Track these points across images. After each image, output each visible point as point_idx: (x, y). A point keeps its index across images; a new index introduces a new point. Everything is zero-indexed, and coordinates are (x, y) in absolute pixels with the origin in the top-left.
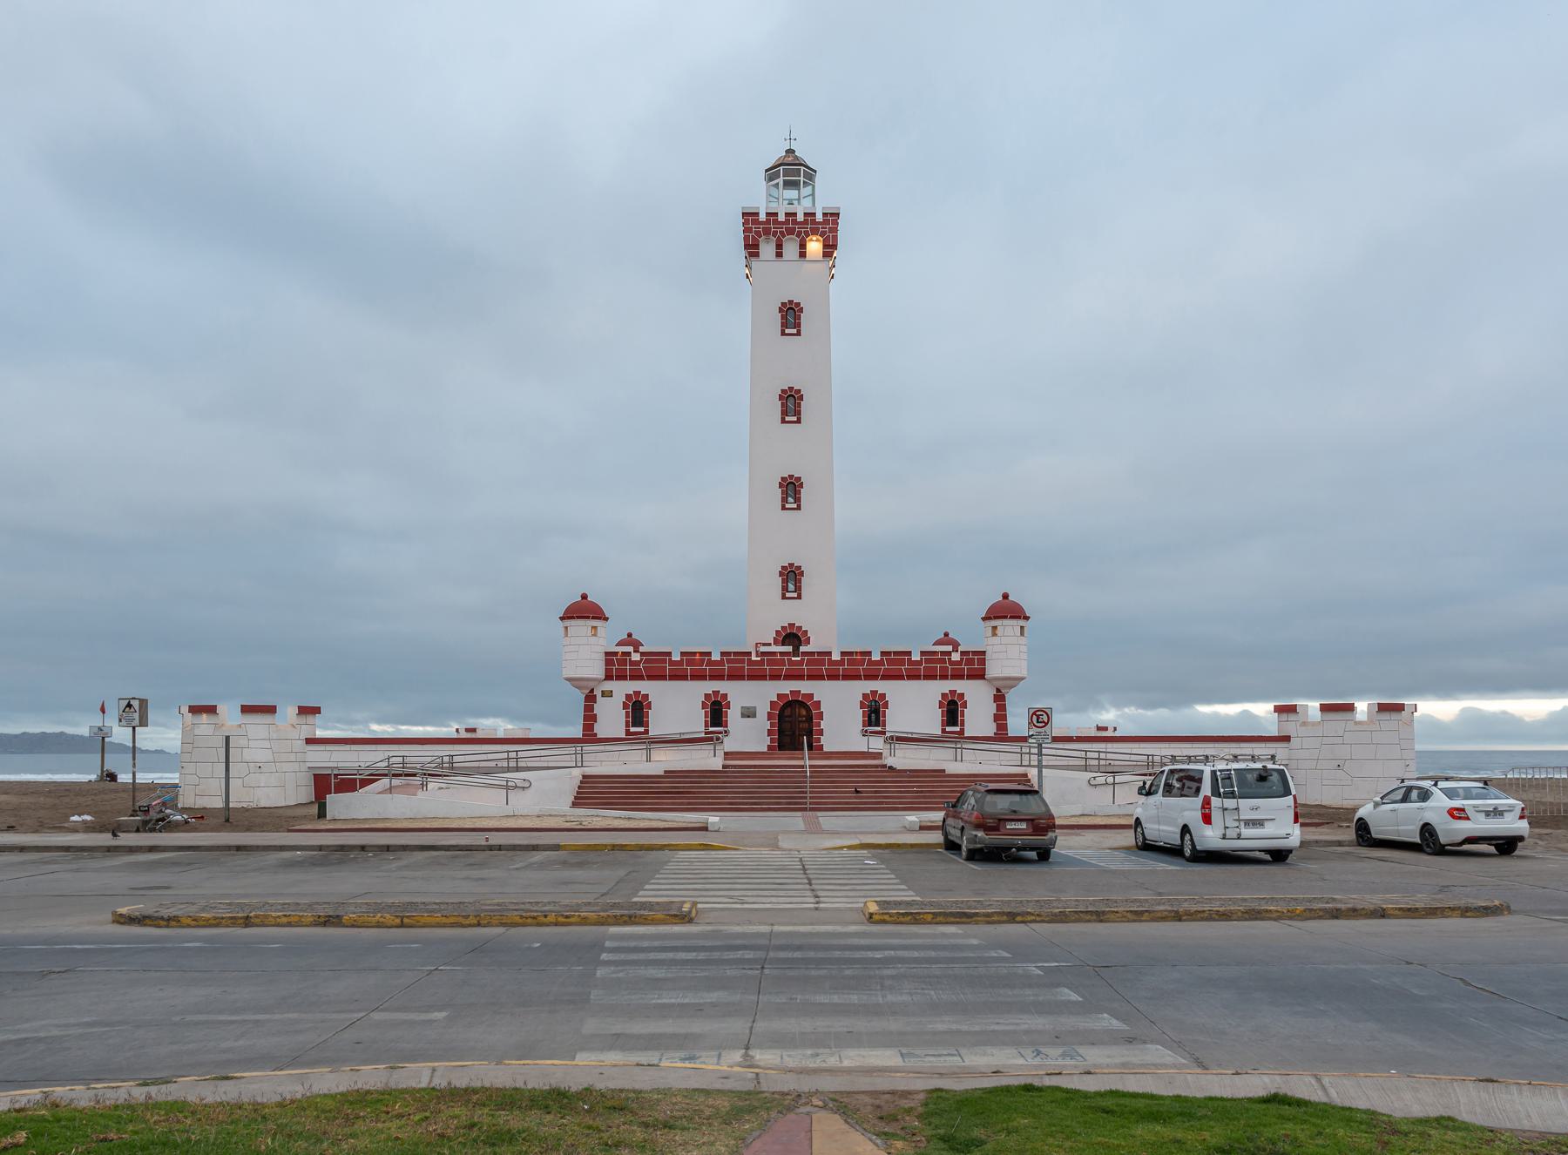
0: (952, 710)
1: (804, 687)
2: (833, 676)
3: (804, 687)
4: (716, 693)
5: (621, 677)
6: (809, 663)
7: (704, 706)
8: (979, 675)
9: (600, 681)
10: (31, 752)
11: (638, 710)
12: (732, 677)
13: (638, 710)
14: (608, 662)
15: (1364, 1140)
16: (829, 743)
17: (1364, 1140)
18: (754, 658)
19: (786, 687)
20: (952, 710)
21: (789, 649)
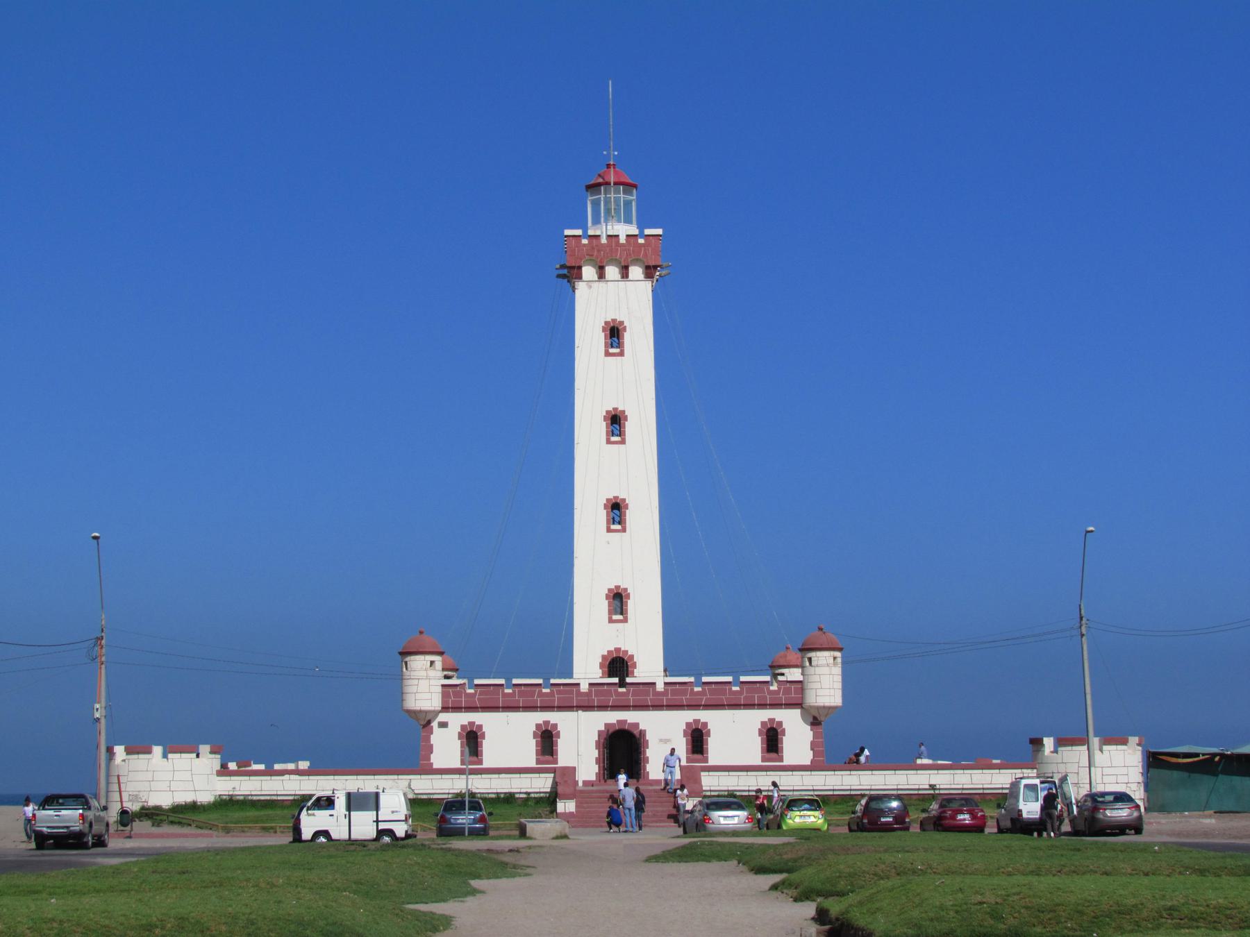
0: (772, 739)
1: (631, 717)
2: (658, 707)
3: (631, 717)
4: (471, 724)
5: (457, 709)
6: (521, 694)
7: (535, 735)
8: (798, 704)
9: (436, 713)
10: (572, 565)
11: (472, 739)
12: (561, 708)
13: (472, 739)
14: (445, 695)
15: (277, 767)
16: (651, 777)
17: (277, 767)
18: (507, 691)
19: (613, 717)
20: (772, 739)
21: (616, 680)
